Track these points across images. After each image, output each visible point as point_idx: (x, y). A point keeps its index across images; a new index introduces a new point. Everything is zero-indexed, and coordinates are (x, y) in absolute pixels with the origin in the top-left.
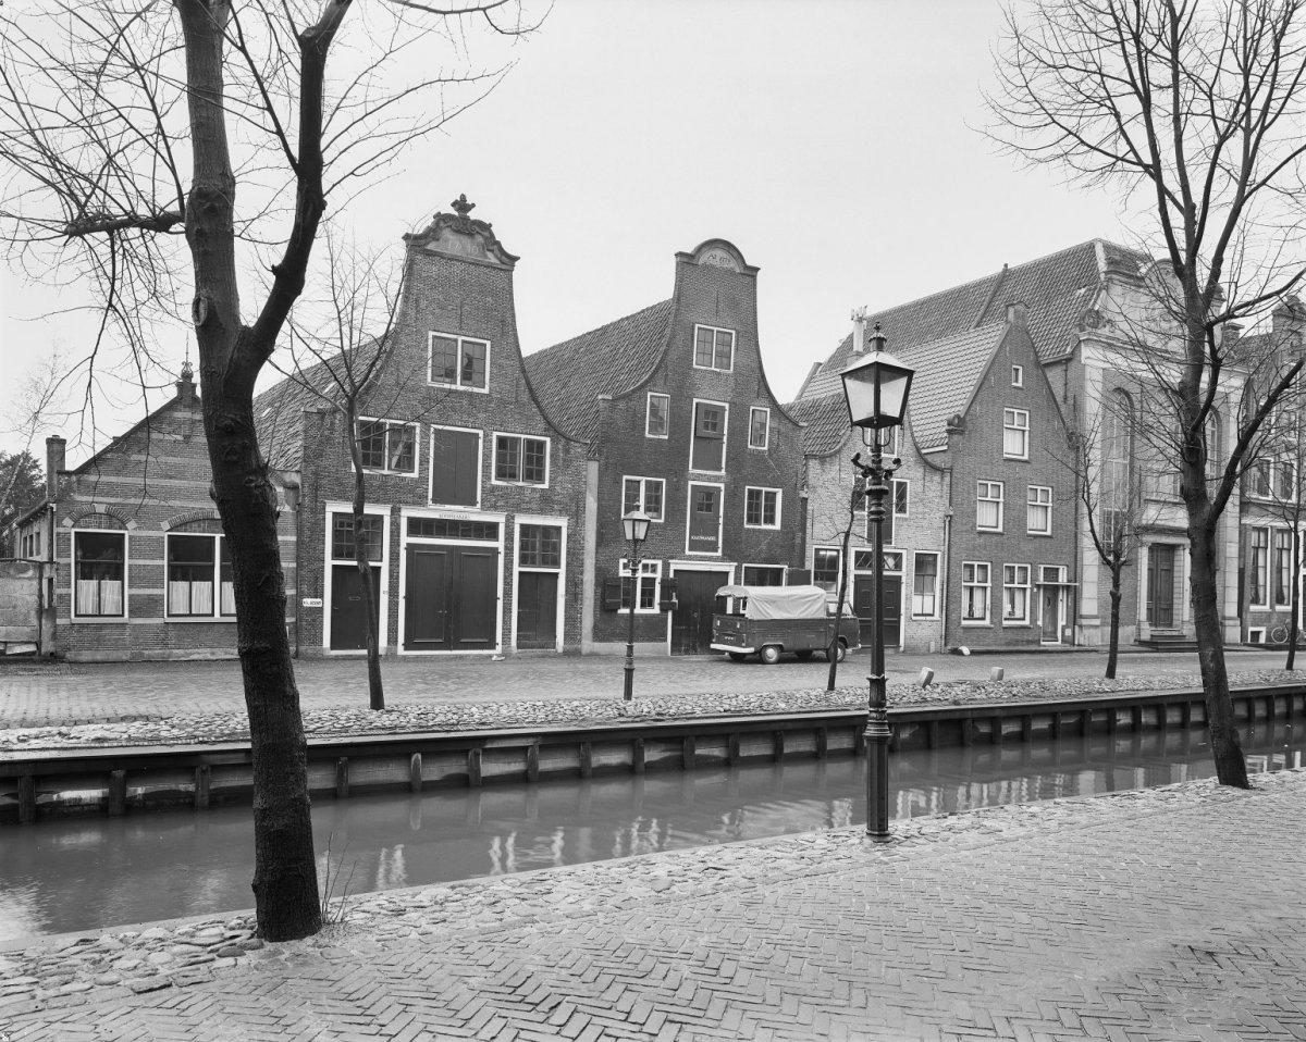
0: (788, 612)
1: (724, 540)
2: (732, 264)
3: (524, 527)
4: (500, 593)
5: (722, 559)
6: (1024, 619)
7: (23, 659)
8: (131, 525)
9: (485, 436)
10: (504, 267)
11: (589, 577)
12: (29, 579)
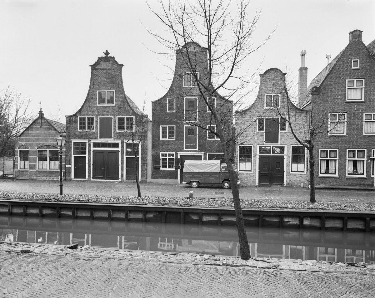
0: (202, 170)
1: (198, 145)
2: (197, 49)
4: (120, 163)
5: (199, 151)
6: (363, 174)
7: (10, 178)
8: (30, 148)
9: (114, 118)
10: (119, 68)
11: (149, 158)
12: (12, 161)
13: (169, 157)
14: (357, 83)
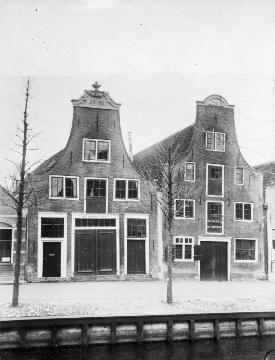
3: (129, 221)
13: (187, 244)
14: (237, 180)
